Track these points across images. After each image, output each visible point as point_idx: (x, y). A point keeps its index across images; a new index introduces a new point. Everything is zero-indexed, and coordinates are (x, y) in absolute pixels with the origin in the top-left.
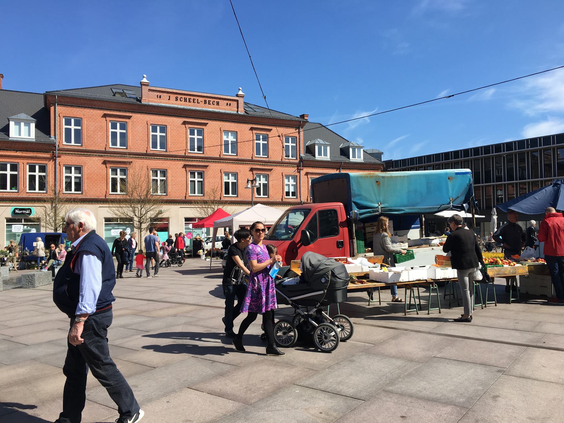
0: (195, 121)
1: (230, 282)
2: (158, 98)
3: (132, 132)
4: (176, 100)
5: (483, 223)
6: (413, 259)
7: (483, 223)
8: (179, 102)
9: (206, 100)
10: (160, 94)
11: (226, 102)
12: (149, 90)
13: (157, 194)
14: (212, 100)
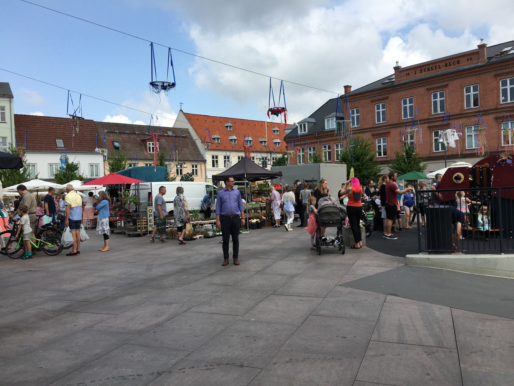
0: (501, 93)
1: (89, 233)
2: (407, 75)
3: (389, 108)
4: (421, 73)
5: (140, 186)
7: (140, 186)
8: (423, 73)
9: (447, 63)
10: (409, 72)
11: (466, 58)
12: (399, 72)
13: (509, 145)
14: (452, 61)
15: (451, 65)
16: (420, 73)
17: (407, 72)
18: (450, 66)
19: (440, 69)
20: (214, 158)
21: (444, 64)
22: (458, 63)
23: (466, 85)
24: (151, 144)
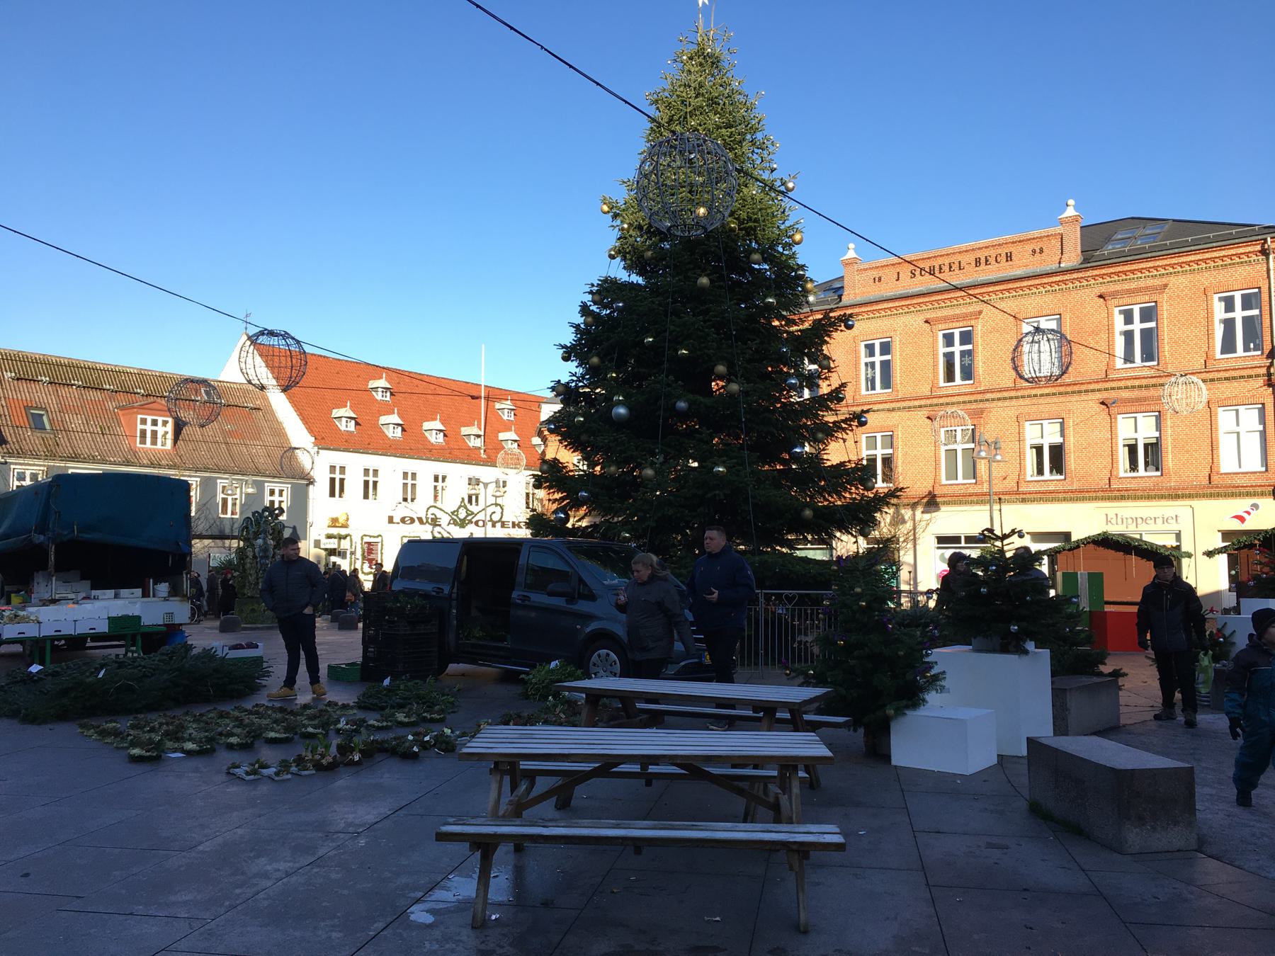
2: (875, 282)
6: (556, 807)
9: (979, 258)
14: (993, 253)
15: (990, 264)
16: (909, 277)
17: (876, 274)
18: (986, 264)
19: (962, 271)
20: (368, 476)
21: (970, 258)
22: (1009, 259)
23: (1029, 315)
24: (149, 422)
